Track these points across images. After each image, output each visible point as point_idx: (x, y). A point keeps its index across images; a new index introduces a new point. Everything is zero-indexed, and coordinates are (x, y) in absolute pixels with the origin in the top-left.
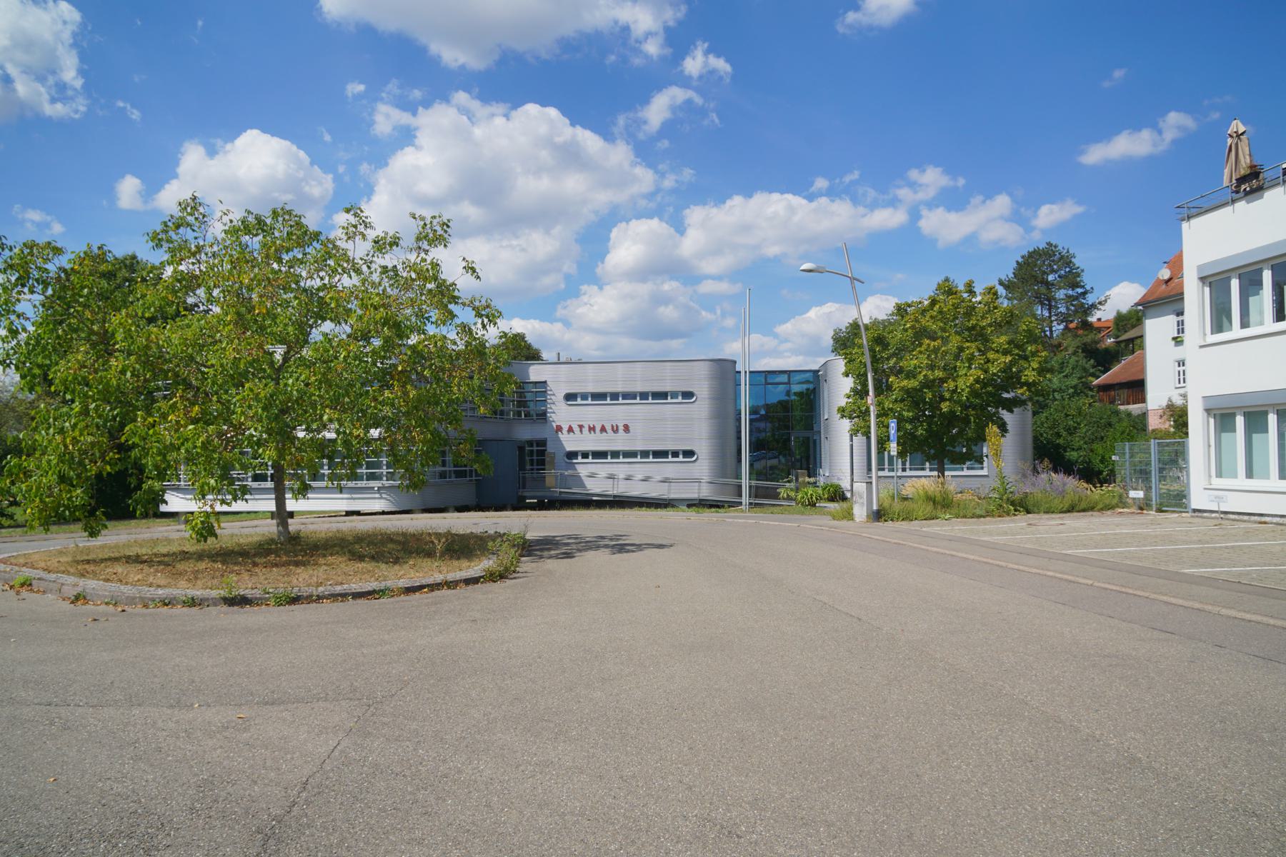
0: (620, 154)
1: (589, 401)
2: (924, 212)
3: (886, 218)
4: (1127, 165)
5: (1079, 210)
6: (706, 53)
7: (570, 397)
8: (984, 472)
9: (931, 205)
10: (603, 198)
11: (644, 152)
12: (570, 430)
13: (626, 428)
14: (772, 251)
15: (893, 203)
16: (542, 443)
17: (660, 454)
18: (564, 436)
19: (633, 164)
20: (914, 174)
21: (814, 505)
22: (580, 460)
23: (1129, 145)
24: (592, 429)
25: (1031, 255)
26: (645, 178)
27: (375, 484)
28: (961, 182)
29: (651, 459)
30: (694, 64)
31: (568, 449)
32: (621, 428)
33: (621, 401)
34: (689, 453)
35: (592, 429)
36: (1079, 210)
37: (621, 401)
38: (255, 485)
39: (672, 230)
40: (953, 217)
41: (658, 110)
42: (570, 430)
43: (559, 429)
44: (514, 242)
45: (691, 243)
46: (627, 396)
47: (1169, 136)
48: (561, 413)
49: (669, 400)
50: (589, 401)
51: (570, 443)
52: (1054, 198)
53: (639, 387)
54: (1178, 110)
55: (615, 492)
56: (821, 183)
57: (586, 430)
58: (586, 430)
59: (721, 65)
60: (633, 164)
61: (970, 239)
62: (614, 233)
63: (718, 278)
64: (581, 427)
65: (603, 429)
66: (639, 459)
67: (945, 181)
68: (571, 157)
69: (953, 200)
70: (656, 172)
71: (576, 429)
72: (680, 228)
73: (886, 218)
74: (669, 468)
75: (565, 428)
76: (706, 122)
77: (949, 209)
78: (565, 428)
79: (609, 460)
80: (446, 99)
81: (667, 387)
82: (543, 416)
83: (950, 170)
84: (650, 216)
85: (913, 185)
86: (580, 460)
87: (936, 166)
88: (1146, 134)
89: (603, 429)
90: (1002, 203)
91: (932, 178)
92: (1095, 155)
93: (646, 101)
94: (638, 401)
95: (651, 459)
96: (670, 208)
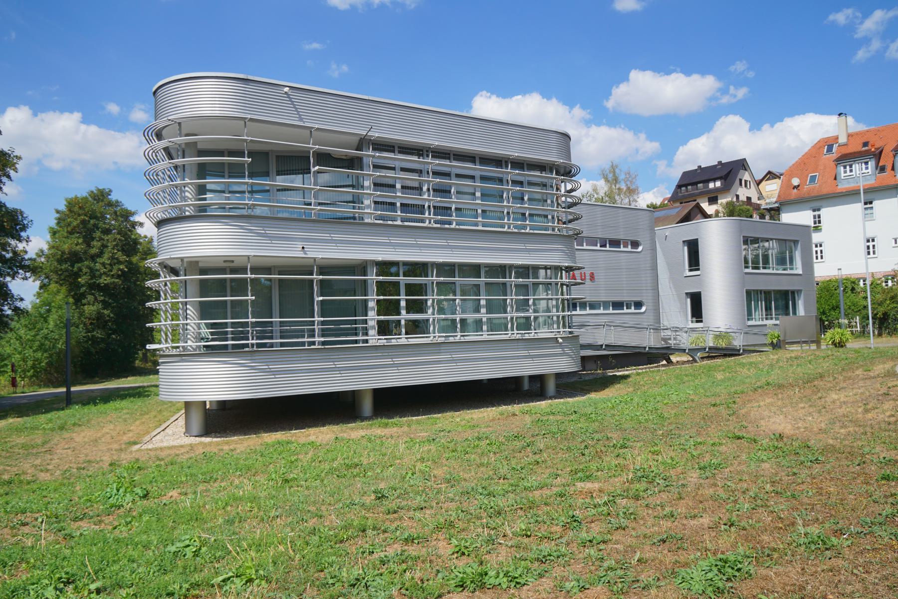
14: (56, 165)
17: (618, 305)
29: (611, 311)
36: (588, 116)
66: (601, 311)
81: (620, 236)
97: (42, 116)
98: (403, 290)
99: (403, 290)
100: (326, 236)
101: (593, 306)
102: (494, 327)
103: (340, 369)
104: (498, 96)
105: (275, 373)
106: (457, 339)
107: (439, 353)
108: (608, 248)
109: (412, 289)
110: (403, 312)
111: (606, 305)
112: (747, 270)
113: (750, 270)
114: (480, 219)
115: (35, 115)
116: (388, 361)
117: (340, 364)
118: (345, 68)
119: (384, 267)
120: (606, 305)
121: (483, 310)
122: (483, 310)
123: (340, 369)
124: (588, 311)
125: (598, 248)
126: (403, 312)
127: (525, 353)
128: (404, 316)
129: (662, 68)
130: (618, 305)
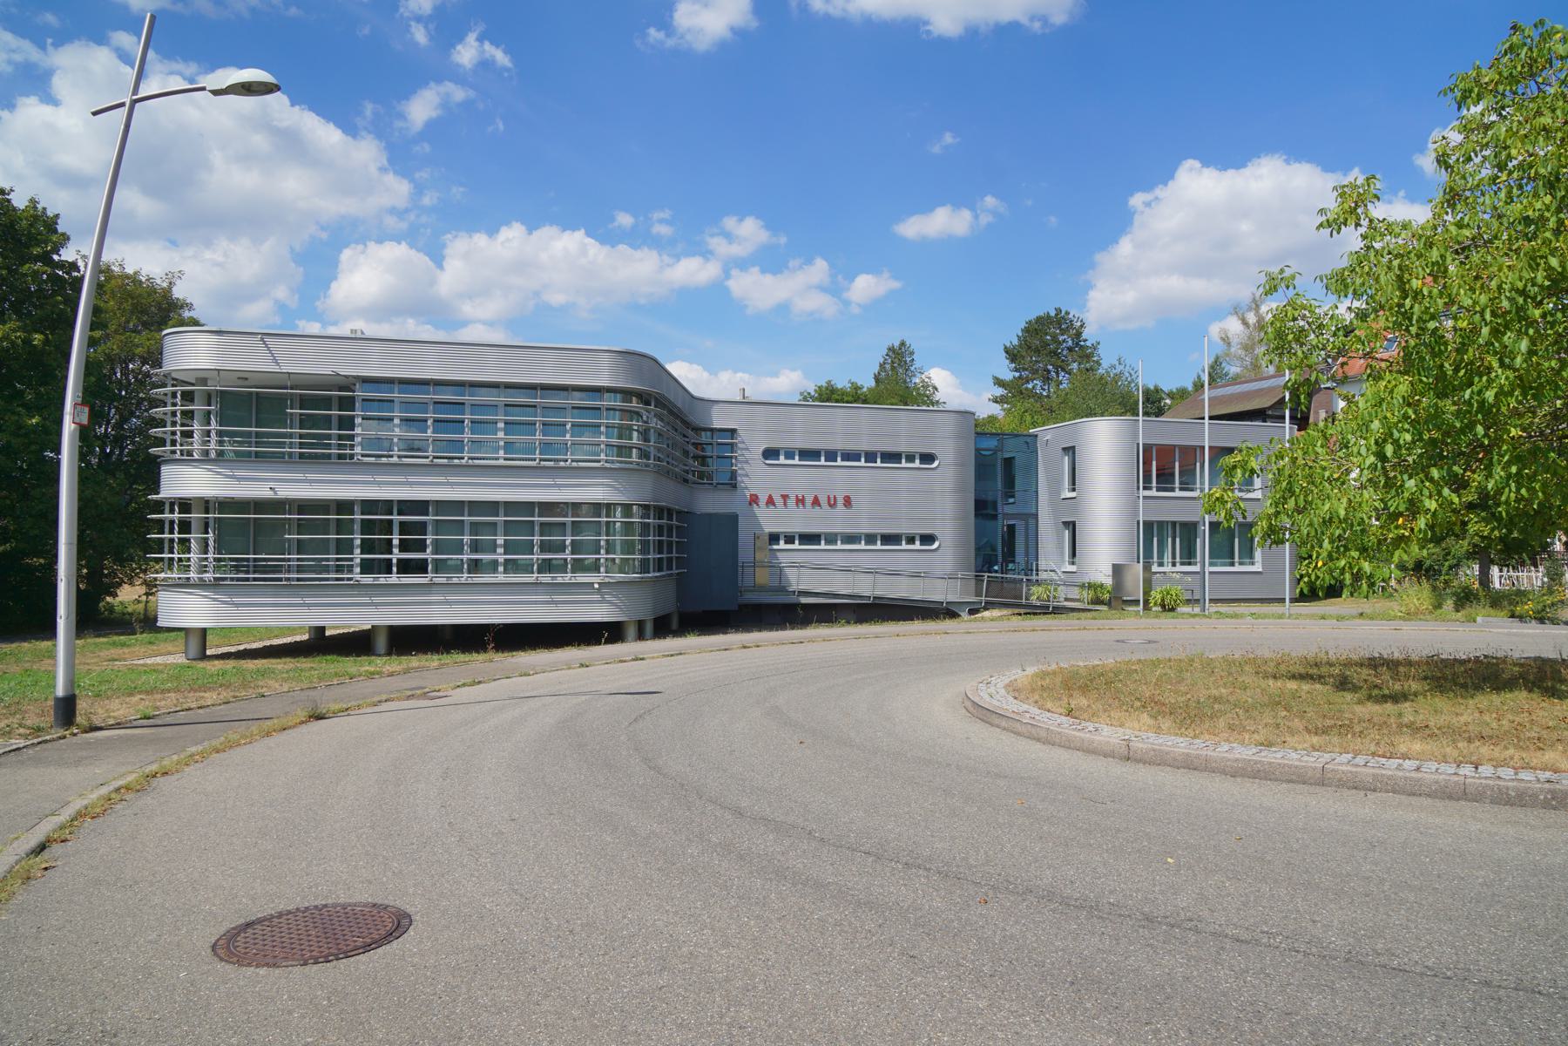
0: (366, 153)
1: (796, 461)
2: (734, 272)
3: (691, 271)
4: (946, 245)
5: (896, 285)
6: (480, 39)
7: (770, 453)
8: (1258, 568)
9: (743, 264)
10: (334, 207)
11: (400, 156)
12: (770, 501)
13: (848, 502)
14: (557, 299)
15: (707, 254)
16: (733, 519)
17: (889, 539)
18: (761, 511)
19: (382, 170)
20: (730, 223)
21: (1173, 610)
22: (782, 545)
23: (942, 222)
24: (800, 501)
25: (1039, 320)
26: (398, 189)
27: (594, 578)
28: (783, 240)
29: (879, 546)
30: (467, 53)
31: (768, 530)
32: (840, 501)
33: (839, 462)
34: (928, 539)
35: (800, 501)
36: (896, 285)
37: (839, 462)
38: (368, 579)
39: (431, 264)
40: (768, 279)
41: (421, 109)
42: (770, 501)
43: (754, 499)
44: (208, 255)
45: (453, 275)
46: (849, 456)
47: (985, 219)
48: (756, 477)
49: (904, 464)
50: (796, 461)
51: (769, 520)
52: (874, 270)
53: (864, 445)
54: (994, 195)
55: (878, 593)
56: (625, 220)
57: (791, 502)
58: (791, 502)
59: (500, 57)
60: (382, 170)
61: (783, 308)
62: (346, 255)
63: (490, 324)
64: (785, 497)
65: (816, 502)
66: (862, 546)
67: (763, 236)
68: (292, 146)
69: (770, 261)
70: (412, 181)
71: (778, 500)
72: (438, 260)
73: (691, 271)
74: (905, 556)
75: (763, 500)
76: (490, 129)
77: (763, 271)
78: (763, 500)
79: (823, 546)
80: (100, 40)
81: (902, 447)
82: (732, 484)
83: (770, 226)
84: (397, 239)
85: (728, 236)
86: (782, 545)
87: (757, 217)
88: (966, 214)
89: (816, 502)
90: (819, 269)
91: (750, 231)
92: (914, 228)
93: (408, 93)
94: (862, 463)
95: (879, 546)
96: (427, 233)
97: (537, 234)
98: (396, 529)
99: (396, 529)
100: (300, 476)
101: (831, 539)
102: (511, 566)
103: (309, 605)
104: (1206, 163)
105: (237, 605)
106: (463, 581)
107: (430, 594)
108: (879, 464)
109: (405, 528)
110: (396, 550)
111: (871, 539)
112: (1147, 493)
113: (1154, 493)
114: (603, 438)
115: (530, 230)
116: (366, 600)
117: (308, 600)
118: (948, 138)
119: (369, 505)
120: (871, 539)
121: (500, 550)
122: (500, 550)
123: (309, 605)
124: (839, 546)
125: (823, 462)
126: (396, 550)
127: (547, 598)
128: (396, 555)
129: (1228, 154)
130: (889, 539)
